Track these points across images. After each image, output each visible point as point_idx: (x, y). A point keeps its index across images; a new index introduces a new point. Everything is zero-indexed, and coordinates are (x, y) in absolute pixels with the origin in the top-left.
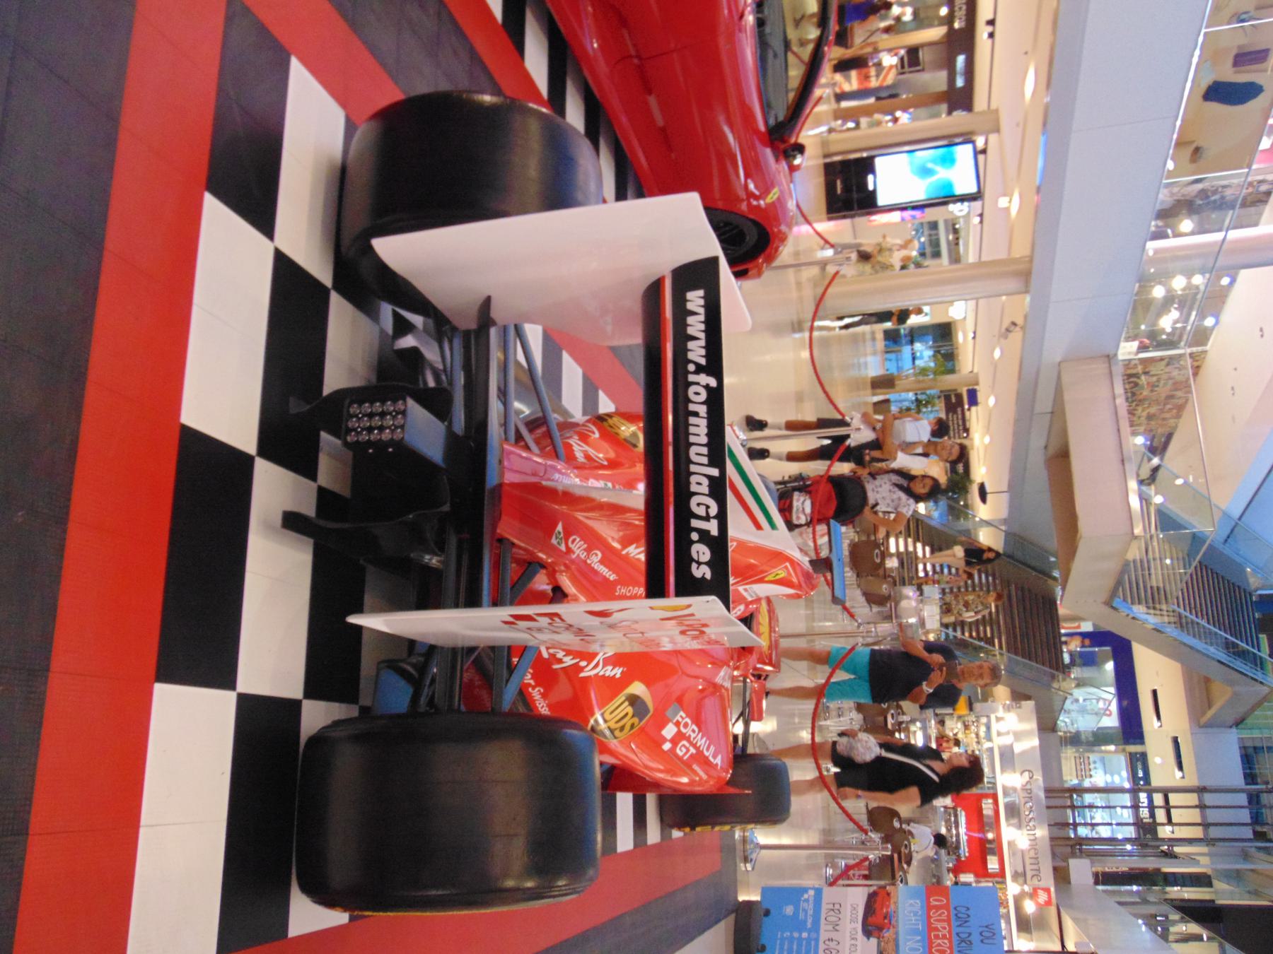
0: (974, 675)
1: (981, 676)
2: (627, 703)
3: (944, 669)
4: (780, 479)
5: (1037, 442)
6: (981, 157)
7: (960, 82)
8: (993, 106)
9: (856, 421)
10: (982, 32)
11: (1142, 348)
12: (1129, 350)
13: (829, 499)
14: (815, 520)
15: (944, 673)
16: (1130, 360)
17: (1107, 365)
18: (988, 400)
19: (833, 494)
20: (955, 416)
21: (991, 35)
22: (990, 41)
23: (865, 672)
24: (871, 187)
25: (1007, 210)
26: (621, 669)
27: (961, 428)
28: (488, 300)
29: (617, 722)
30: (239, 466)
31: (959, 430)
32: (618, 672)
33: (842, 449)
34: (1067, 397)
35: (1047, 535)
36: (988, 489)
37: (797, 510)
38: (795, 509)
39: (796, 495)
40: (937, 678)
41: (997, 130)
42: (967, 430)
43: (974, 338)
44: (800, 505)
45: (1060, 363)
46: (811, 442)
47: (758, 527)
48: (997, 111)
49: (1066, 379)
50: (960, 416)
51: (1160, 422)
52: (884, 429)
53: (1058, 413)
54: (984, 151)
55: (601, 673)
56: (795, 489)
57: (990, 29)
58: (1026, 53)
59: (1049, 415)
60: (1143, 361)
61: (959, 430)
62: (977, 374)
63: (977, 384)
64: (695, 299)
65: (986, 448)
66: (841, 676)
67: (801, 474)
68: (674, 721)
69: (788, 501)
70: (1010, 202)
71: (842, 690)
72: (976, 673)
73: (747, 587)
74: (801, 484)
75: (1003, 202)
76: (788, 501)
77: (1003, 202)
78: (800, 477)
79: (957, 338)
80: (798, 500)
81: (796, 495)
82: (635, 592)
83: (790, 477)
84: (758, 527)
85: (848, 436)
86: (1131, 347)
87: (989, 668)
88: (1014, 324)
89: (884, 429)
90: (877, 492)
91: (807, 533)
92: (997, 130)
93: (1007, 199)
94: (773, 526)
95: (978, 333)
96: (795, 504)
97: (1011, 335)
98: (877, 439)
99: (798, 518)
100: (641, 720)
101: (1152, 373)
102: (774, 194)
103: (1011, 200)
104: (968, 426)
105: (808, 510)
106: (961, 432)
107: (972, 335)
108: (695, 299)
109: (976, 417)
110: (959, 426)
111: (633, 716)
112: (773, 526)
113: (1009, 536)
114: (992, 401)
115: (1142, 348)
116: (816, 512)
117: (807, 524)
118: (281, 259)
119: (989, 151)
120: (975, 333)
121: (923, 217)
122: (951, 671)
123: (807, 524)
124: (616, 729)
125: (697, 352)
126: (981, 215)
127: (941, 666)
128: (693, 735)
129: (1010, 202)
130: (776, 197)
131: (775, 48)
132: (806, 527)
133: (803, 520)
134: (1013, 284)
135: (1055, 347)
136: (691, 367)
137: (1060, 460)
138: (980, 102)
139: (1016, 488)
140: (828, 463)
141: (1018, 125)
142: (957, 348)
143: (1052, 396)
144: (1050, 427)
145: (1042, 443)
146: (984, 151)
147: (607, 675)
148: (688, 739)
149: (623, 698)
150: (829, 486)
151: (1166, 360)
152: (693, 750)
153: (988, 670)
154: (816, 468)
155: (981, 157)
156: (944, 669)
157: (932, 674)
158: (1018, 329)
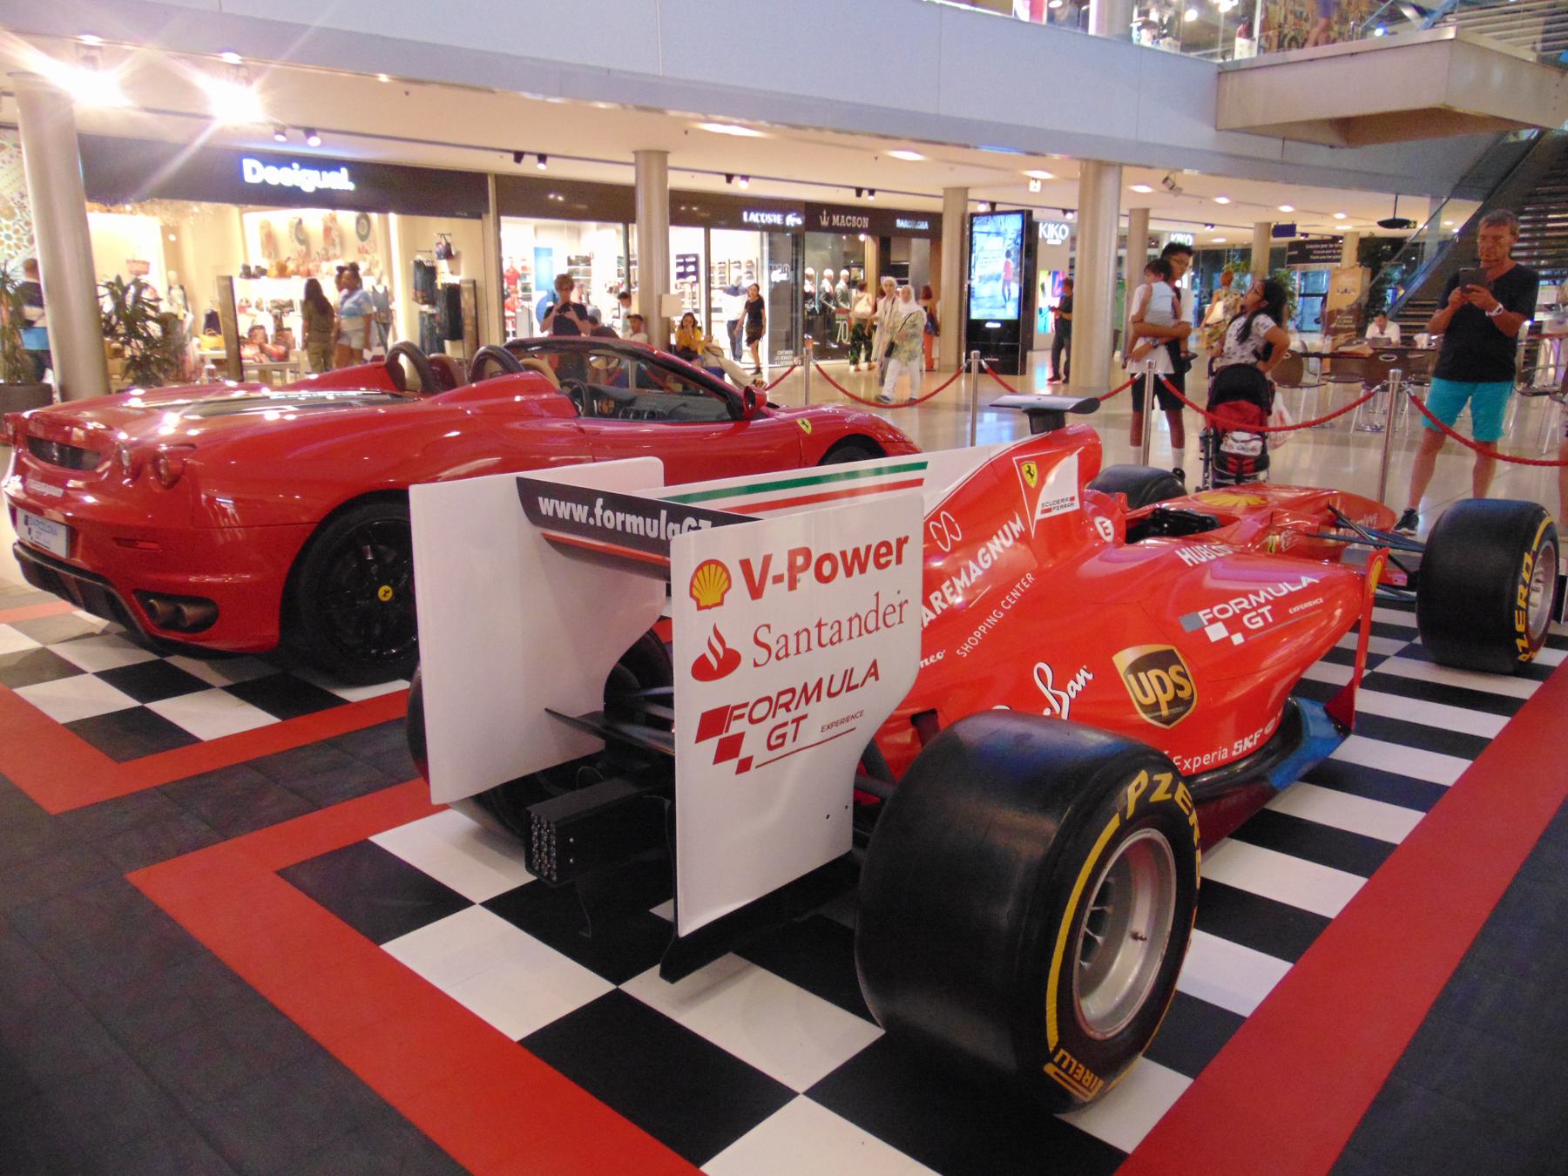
0: (1493, 247)
1: (1496, 238)
2: (1142, 675)
3: (1468, 286)
4: (1202, 463)
5: (1320, 156)
6: (999, 208)
7: (924, 226)
8: (941, 193)
9: (1135, 369)
10: (867, 200)
11: (1248, 33)
12: (1245, 48)
13: (1237, 409)
14: (1262, 428)
15: (1474, 286)
16: (1260, 47)
17: (1230, 76)
18: (1285, 212)
19: (1231, 403)
20: (1315, 252)
21: (872, 192)
22: (876, 193)
23: (1466, 386)
24: (998, 325)
25: (1044, 182)
26: (1082, 671)
27: (1331, 246)
28: (546, 710)
29: (1165, 690)
30: (615, 1009)
31: (1334, 248)
32: (1083, 677)
33: (1169, 386)
34: (1258, 121)
35: (1464, 149)
36: (1389, 216)
37: (1243, 449)
38: (1242, 452)
39: (1223, 448)
40: (1481, 296)
41: (966, 190)
42: (1335, 239)
43: (1212, 226)
44: (1238, 445)
45: (1218, 130)
46: (1159, 419)
47: (919, 482)
48: (946, 190)
49: (1237, 122)
50: (1317, 246)
51: (1352, 8)
52: (1156, 336)
53: (1287, 132)
54: (993, 205)
55: (1073, 695)
56: (1217, 449)
57: (865, 193)
58: (876, 158)
59: (1287, 142)
60: (1264, 28)
61: (1334, 248)
62: (1256, 224)
63: (1269, 224)
64: (546, 506)
65: (1351, 217)
66: (1464, 423)
67: (1201, 438)
68: (1206, 623)
69: (1230, 459)
70: (1036, 180)
71: (1488, 422)
72: (1491, 244)
73: (1039, 508)
74: (1213, 440)
75: (1035, 187)
76: (1230, 459)
77: (1035, 187)
78: (1204, 440)
79: (1219, 245)
80: (1231, 447)
81: (1223, 448)
82: (979, 636)
83: (1202, 451)
84: (919, 482)
85: (1156, 376)
86: (1241, 46)
87: (1488, 227)
88: (1166, 180)
89: (1156, 336)
90: (1234, 353)
91: (1276, 439)
92: (966, 190)
93: (1032, 183)
94: (923, 466)
95: (1207, 222)
96: (1235, 451)
97: (1179, 184)
98: (1166, 344)
99: (1253, 449)
100: (1179, 663)
101: (1282, 20)
102: (804, 423)
103: (1033, 179)
104: (1330, 238)
105: (1245, 436)
106: (1336, 245)
107: (1209, 227)
108: (546, 506)
109: (1312, 226)
110: (1328, 248)
111: (1167, 672)
112: (923, 466)
113: (1461, 190)
114: (1286, 209)
115: (1248, 33)
116: (1249, 426)
117: (1263, 438)
118: (498, 905)
119: (993, 199)
120: (1207, 225)
121: (1063, 273)
122: (1477, 278)
123: (1263, 438)
124: (1176, 694)
125: (580, 513)
126: (1065, 211)
127: (1464, 290)
128: (1245, 605)
129: (1036, 180)
130: (807, 422)
131: (678, 404)
132: (1267, 441)
133: (1258, 444)
134: (1109, 182)
135: (1201, 135)
136: (591, 521)
137: (1350, 129)
138: (935, 205)
139: (1397, 185)
140: (1203, 404)
141: (952, 169)
142: (1234, 245)
143: (1261, 139)
144: (1299, 140)
145: (1324, 151)
146: (993, 205)
147: (1080, 689)
148: (1245, 611)
149: (1131, 678)
150: (1221, 407)
151: (1268, 4)
152: (1265, 610)
153: (1491, 228)
154: (1194, 424)
155: (999, 208)
156: (1468, 286)
157: (1475, 303)
158: (1172, 177)
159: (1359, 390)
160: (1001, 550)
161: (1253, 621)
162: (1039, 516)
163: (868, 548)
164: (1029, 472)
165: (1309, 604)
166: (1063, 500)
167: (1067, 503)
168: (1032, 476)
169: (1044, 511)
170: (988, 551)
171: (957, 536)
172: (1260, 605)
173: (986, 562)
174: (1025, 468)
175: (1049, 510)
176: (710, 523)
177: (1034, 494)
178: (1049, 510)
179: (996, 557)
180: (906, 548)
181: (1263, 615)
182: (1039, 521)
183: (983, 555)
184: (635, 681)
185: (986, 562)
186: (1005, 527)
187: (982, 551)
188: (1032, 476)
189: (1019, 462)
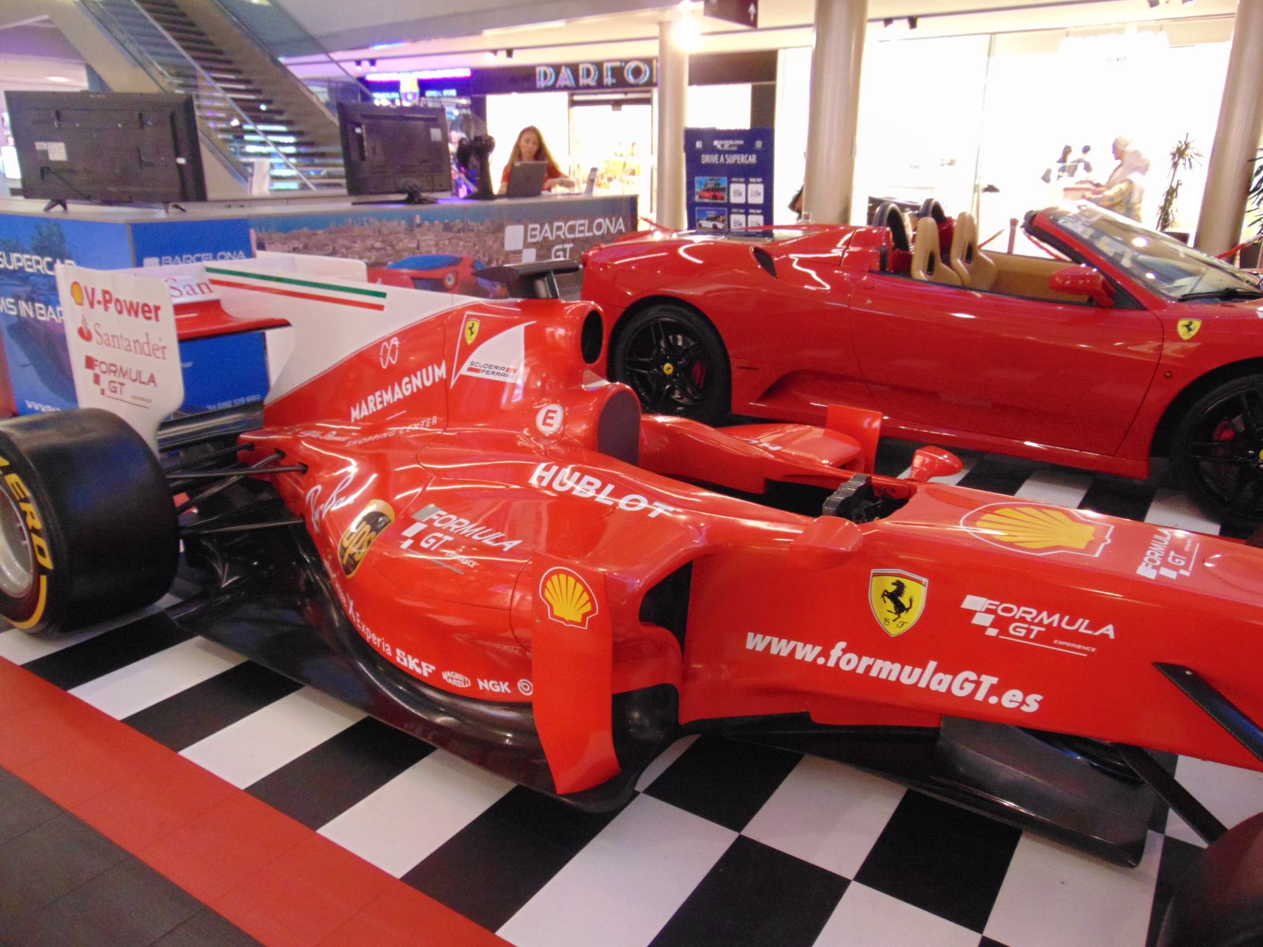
47: (380, 308)
73: (467, 364)
94: (383, 295)
112: (383, 295)
159: (894, 611)
160: (420, 386)
161: (1018, 629)
162: (464, 371)
163: (138, 304)
164: (471, 328)
165: (929, 794)
166: (496, 367)
167: (502, 372)
168: (472, 333)
169: (470, 369)
170: (411, 382)
171: (394, 360)
172: (1040, 624)
173: (407, 390)
174: (469, 324)
175: (477, 371)
176: (1077, 496)
177: (467, 350)
178: (477, 371)
179: (415, 390)
180: (160, 313)
181: (1030, 631)
182: (462, 376)
183: (407, 383)
184: (878, 480)
185: (407, 390)
186: (430, 368)
187: (406, 379)
188: (472, 333)
189: (469, 316)
